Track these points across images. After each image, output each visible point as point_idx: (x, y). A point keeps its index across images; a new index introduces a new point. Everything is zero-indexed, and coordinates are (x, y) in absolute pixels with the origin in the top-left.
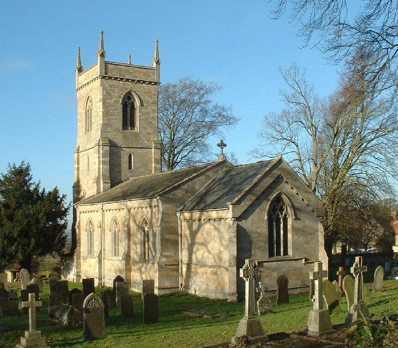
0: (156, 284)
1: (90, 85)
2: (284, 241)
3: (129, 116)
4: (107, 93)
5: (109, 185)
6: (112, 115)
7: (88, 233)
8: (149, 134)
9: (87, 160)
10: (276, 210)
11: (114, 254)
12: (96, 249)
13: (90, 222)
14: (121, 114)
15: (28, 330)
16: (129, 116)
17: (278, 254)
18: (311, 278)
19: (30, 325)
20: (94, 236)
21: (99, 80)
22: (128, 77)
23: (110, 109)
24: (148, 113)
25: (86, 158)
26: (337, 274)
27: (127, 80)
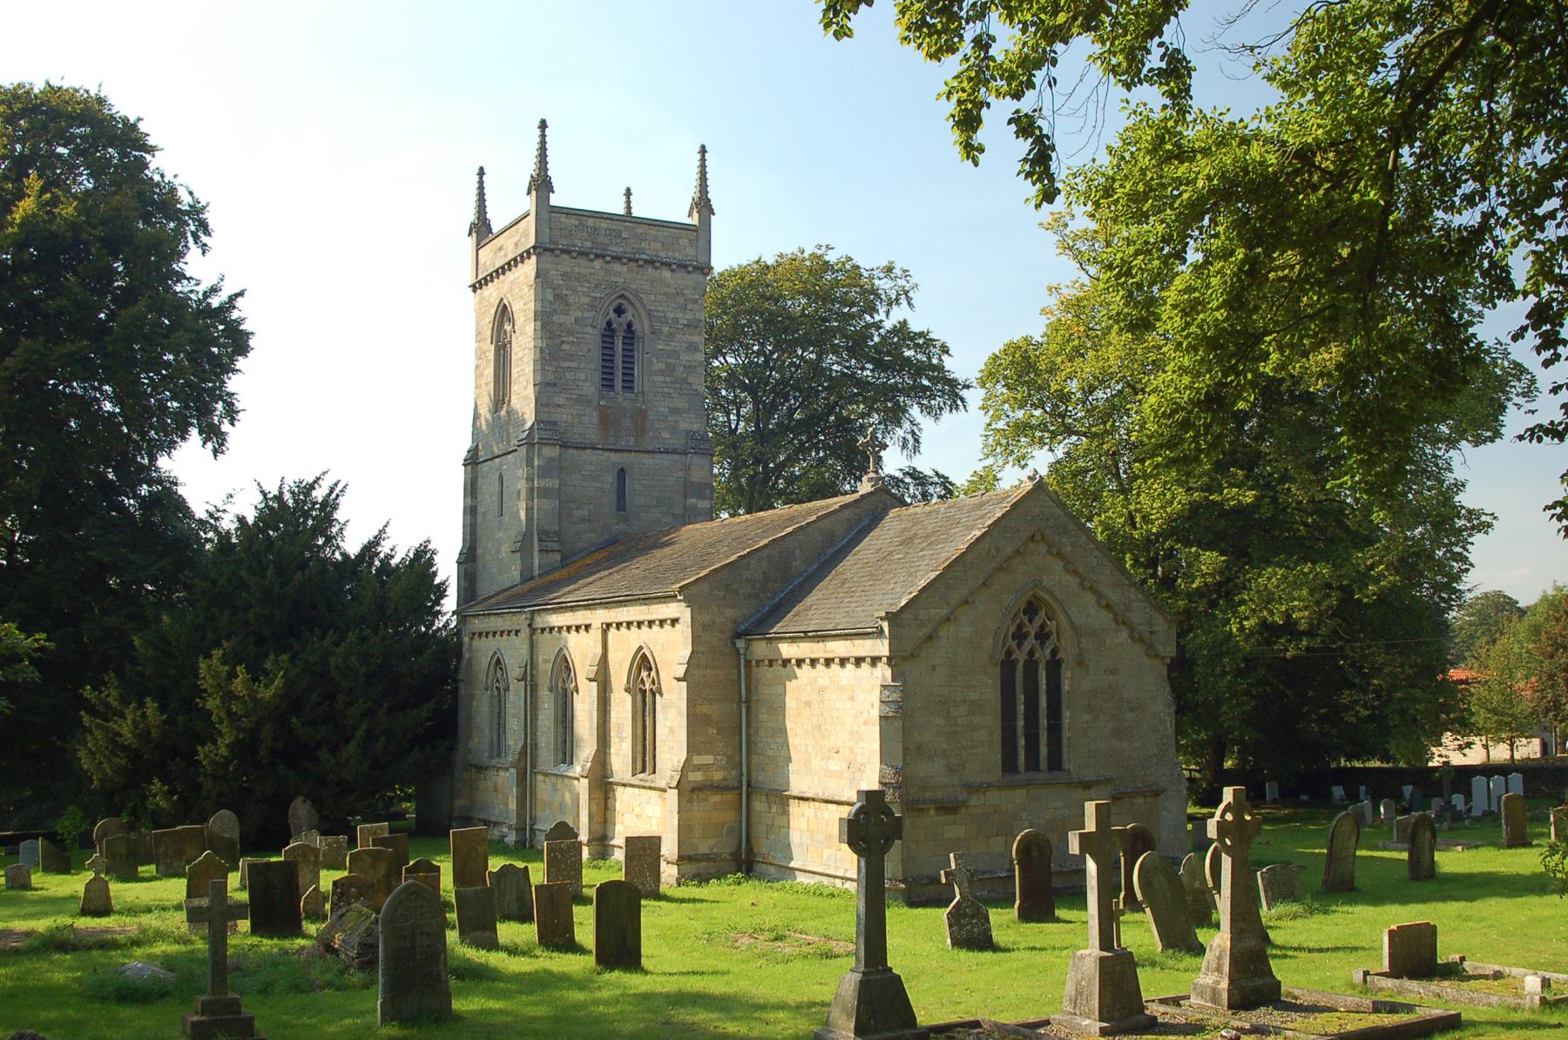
0: (669, 848)
1: (510, 276)
2: (1050, 728)
3: (619, 360)
4: (557, 296)
5: (558, 557)
6: (570, 357)
7: (492, 696)
8: (676, 411)
9: (497, 484)
10: (1025, 636)
11: (560, 756)
12: (514, 741)
13: (498, 661)
14: (596, 354)
15: (1430, 36)
16: (619, 360)
17: (1033, 764)
18: (1074, 847)
19: (1262, 894)
20: (509, 705)
21: (534, 258)
22: (617, 249)
23: (563, 342)
24: (675, 354)
25: (495, 478)
26: (1074, 847)
27: (617, 258)
